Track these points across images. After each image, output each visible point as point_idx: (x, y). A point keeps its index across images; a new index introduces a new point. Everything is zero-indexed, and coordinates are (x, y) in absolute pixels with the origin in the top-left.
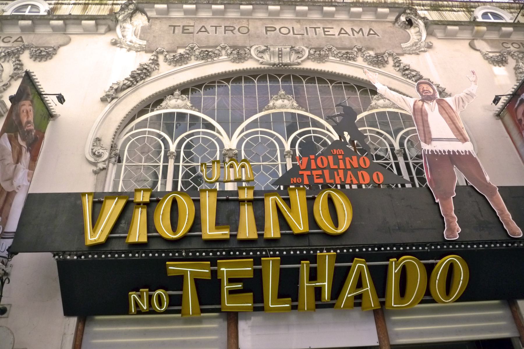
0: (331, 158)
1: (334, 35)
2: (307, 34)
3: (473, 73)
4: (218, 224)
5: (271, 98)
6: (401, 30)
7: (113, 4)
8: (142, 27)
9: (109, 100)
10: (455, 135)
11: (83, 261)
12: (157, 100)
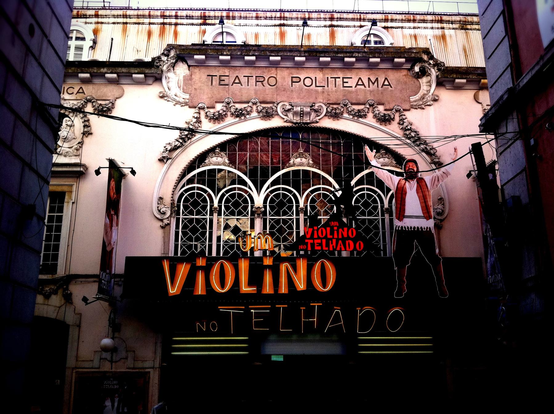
0: (328, 229)
1: (351, 87)
2: (328, 86)
3: (455, 149)
4: (250, 284)
5: (292, 155)
6: (414, 79)
7: (150, 24)
8: (184, 77)
9: (165, 161)
10: (423, 213)
12: (201, 158)
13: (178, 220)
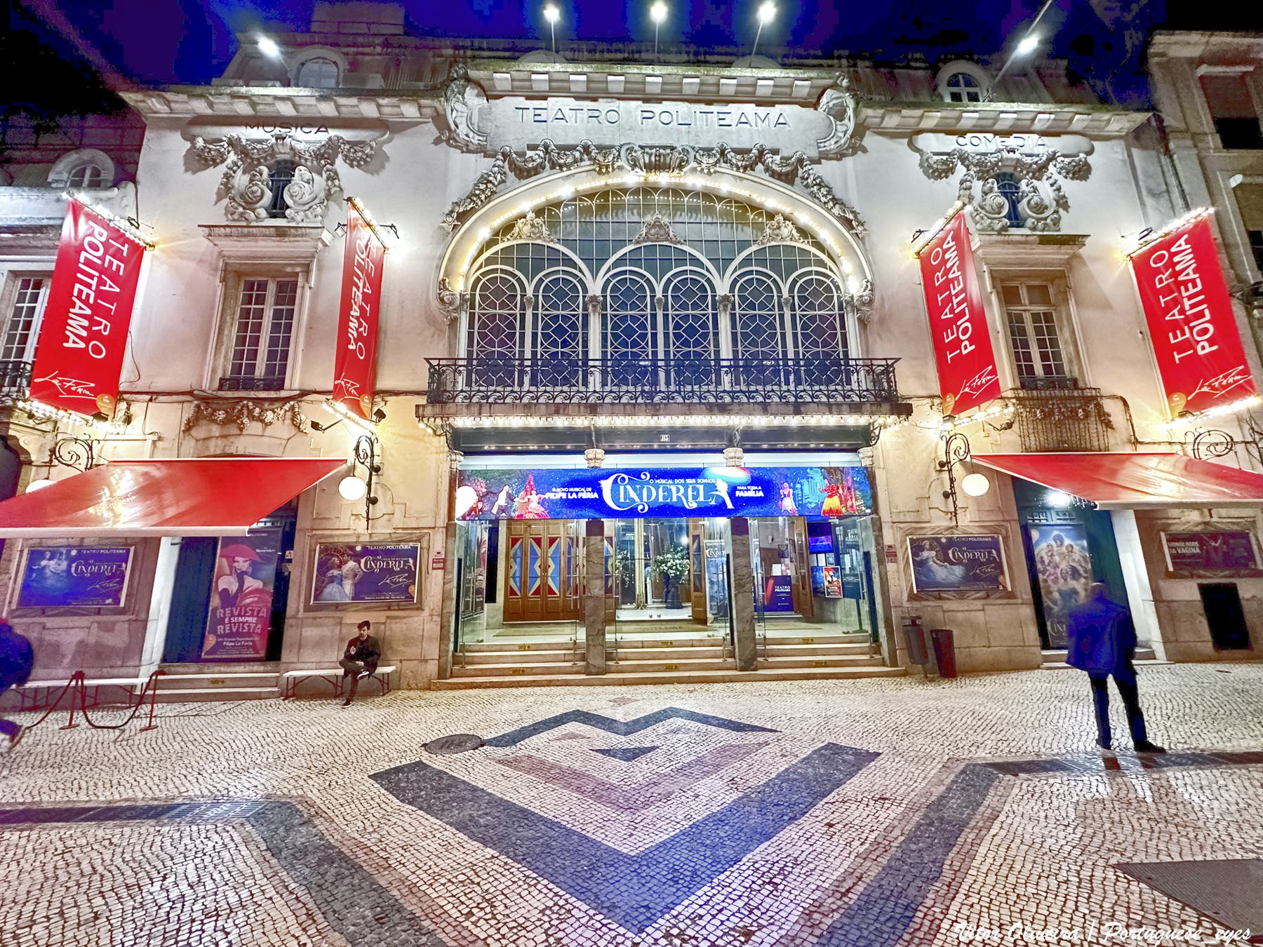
13: (472, 316)
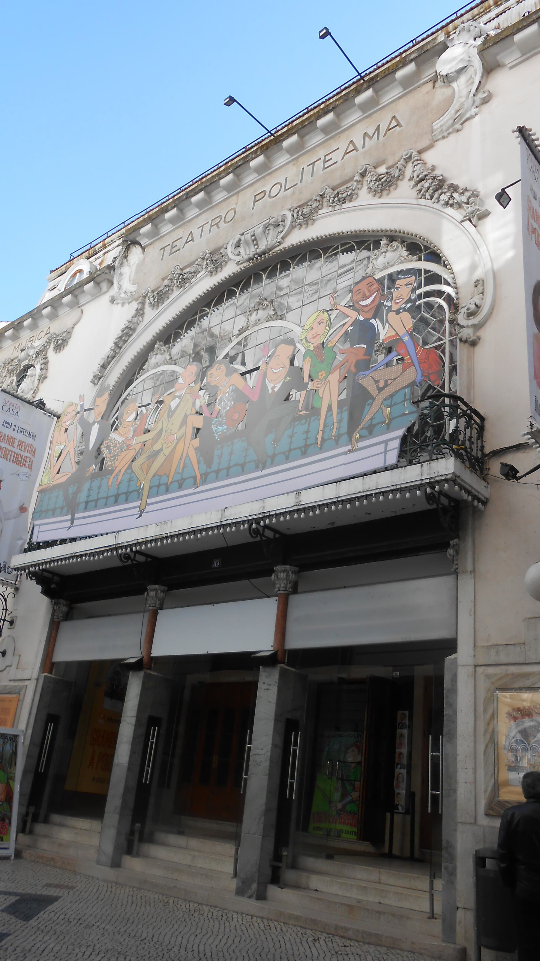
11: (188, 540)
